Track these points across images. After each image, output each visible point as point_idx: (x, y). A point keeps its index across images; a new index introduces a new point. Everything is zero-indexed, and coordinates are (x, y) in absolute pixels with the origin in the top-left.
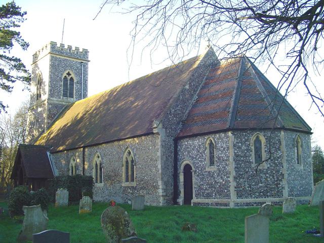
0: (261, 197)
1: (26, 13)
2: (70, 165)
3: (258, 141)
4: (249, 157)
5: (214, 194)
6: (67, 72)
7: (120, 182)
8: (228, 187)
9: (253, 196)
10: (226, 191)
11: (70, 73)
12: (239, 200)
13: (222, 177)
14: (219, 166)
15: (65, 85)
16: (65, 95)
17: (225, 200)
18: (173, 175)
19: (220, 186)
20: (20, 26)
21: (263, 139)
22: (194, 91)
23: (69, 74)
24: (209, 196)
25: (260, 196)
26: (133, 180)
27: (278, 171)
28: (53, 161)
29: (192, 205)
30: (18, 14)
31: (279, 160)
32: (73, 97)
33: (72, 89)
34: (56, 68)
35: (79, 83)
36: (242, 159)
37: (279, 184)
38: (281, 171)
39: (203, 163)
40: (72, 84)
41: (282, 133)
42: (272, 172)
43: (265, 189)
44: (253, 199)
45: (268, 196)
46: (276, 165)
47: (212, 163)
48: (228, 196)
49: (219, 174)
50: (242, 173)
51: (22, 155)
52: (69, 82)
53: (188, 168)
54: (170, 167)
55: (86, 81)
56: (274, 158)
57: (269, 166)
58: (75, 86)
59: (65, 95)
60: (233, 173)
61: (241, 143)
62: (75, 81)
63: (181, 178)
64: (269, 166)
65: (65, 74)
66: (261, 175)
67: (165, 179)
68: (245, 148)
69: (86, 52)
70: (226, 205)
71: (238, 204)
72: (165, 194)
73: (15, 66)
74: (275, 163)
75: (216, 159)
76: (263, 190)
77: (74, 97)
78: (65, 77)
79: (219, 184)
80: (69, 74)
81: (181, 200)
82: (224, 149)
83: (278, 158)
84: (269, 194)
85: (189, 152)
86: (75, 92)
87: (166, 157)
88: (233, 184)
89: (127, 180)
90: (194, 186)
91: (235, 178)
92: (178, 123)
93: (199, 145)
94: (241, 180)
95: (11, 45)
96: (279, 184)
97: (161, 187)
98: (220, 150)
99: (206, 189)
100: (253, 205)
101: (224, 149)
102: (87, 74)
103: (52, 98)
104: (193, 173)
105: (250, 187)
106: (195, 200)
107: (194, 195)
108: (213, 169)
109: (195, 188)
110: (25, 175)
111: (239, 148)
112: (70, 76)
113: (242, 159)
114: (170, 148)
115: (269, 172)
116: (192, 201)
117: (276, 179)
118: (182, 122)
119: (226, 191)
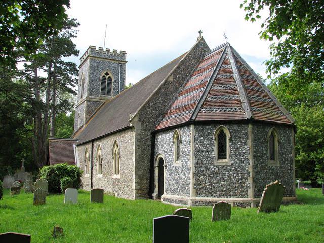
0: (223, 196)
1: (79, 24)
4: (212, 152)
6: (106, 72)
9: (214, 194)
10: (187, 188)
11: (109, 73)
15: (103, 84)
16: (103, 93)
17: (185, 198)
20: (76, 37)
23: (107, 74)
25: (221, 196)
26: (109, 93)
30: (75, 26)
31: (245, 156)
32: (110, 95)
34: (94, 69)
40: (110, 83)
41: (250, 126)
42: (236, 169)
43: (228, 187)
44: (214, 199)
46: (242, 162)
47: (178, 159)
50: (202, 169)
53: (161, 161)
54: (146, 161)
59: (103, 93)
62: (113, 80)
64: (233, 162)
65: (104, 74)
66: (224, 172)
67: (140, 173)
69: (124, 53)
71: (196, 202)
72: (139, 187)
75: (181, 154)
76: (225, 189)
77: (112, 94)
78: (104, 77)
80: (107, 74)
81: (155, 195)
83: (244, 153)
84: (231, 193)
86: (112, 90)
87: (142, 151)
88: (191, 181)
90: (164, 180)
96: (244, 183)
97: (134, 181)
102: (124, 74)
104: (165, 168)
105: (211, 185)
108: (178, 164)
109: (165, 183)
114: (147, 141)
115: (233, 169)
117: (240, 177)
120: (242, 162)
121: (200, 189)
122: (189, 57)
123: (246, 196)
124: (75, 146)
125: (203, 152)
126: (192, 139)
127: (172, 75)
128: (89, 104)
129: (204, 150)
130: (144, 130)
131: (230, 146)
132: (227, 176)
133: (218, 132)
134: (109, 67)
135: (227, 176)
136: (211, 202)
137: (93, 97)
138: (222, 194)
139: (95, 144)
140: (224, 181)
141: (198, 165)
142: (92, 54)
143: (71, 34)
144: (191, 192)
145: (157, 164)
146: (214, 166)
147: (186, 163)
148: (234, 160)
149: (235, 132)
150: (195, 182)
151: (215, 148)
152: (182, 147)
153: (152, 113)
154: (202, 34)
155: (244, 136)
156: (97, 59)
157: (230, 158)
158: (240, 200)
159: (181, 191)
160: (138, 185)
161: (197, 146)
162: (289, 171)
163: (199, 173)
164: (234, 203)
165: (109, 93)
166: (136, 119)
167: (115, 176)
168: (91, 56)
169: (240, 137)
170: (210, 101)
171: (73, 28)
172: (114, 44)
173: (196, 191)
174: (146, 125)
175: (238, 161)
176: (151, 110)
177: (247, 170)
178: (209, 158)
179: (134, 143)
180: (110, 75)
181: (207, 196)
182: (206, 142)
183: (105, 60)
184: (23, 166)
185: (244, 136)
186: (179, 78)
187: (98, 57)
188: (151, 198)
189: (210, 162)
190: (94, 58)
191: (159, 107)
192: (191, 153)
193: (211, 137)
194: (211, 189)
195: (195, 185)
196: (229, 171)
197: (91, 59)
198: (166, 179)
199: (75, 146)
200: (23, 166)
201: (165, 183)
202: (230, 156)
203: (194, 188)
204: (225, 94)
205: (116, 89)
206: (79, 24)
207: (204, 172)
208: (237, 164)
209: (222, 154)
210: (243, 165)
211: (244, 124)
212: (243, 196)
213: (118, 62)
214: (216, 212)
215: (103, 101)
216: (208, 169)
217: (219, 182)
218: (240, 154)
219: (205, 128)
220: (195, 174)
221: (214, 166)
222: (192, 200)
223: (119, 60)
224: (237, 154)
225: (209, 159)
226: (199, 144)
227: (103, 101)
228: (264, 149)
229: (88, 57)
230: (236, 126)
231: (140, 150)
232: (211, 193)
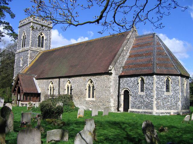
2: (49, 86)
3: (168, 81)
5: (143, 107)
7: (85, 97)
8: (152, 104)
9: (165, 109)
10: (150, 106)
11: (42, 33)
12: (158, 111)
13: (148, 99)
14: (146, 92)
15: (39, 40)
16: (39, 46)
17: (150, 111)
18: (118, 96)
19: (146, 103)
22: (128, 51)
24: (139, 108)
27: (177, 97)
28: (37, 83)
29: (129, 112)
36: (160, 89)
37: (177, 103)
38: (178, 97)
39: (137, 90)
40: (43, 40)
42: (174, 97)
43: (171, 105)
45: (172, 109)
47: (142, 90)
48: (152, 108)
49: (146, 97)
51: (20, 79)
52: (41, 39)
56: (176, 90)
57: (173, 93)
58: (44, 41)
59: (39, 46)
60: (155, 97)
61: (160, 81)
62: (45, 38)
63: (122, 97)
68: (161, 84)
70: (150, 113)
73: (6, 27)
74: (175, 92)
75: (144, 89)
78: (40, 36)
79: (146, 102)
80: (41, 34)
82: (150, 83)
84: (172, 108)
85: (128, 84)
88: (155, 102)
89: (89, 97)
91: (156, 99)
92: (120, 68)
93: (135, 81)
94: (159, 100)
95: (4, 15)
96: (177, 103)
98: (147, 84)
99: (138, 104)
100: (164, 114)
101: (150, 83)
103: (32, 47)
104: (130, 95)
105: (163, 104)
106: (130, 109)
107: (130, 107)
110: (22, 91)
111: (159, 83)
112: (42, 36)
113: (160, 89)
116: (129, 110)
118: (123, 67)
119: (150, 106)
124: (34, 79)
128: (31, 52)
129: (160, 87)
130: (116, 75)
145: (122, 92)
148: (173, 93)
151: (165, 87)
165: (42, 47)
168: (33, 22)
180: (43, 35)
196: (171, 98)
198: (131, 101)
199: (34, 79)
205: (46, 44)
218: (176, 90)
224: (175, 91)
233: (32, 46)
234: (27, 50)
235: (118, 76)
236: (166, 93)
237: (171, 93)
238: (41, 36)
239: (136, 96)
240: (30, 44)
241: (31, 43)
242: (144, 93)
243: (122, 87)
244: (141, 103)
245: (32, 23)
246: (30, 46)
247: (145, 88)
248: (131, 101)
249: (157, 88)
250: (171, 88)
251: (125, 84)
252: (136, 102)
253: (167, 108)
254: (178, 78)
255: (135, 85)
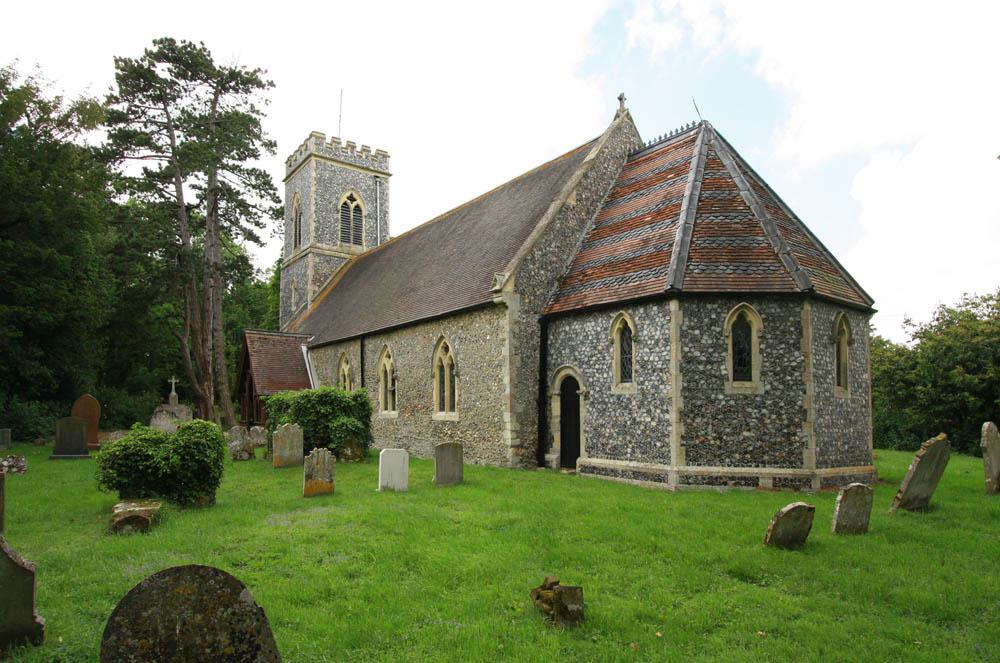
1: (271, 84)
3: (742, 327)
5: (629, 450)
6: (348, 194)
7: (428, 410)
9: (727, 460)
10: (658, 444)
11: (355, 196)
13: (649, 412)
14: (642, 383)
15: (345, 219)
16: (345, 239)
17: (657, 467)
19: (644, 432)
21: (756, 322)
22: (588, 213)
24: (615, 453)
25: (743, 462)
26: (452, 408)
27: (791, 403)
31: (797, 374)
33: (358, 228)
35: (372, 216)
36: (701, 368)
38: (799, 403)
39: (605, 376)
40: (358, 219)
41: (807, 307)
42: (775, 404)
43: (759, 444)
46: (789, 387)
47: (626, 376)
48: (664, 457)
49: (642, 402)
50: (699, 403)
53: (570, 386)
55: (385, 213)
57: (768, 387)
59: (345, 239)
63: (556, 407)
64: (768, 387)
66: (749, 410)
67: (520, 409)
68: (710, 342)
69: (385, 156)
71: (688, 477)
72: (518, 442)
75: (635, 367)
76: (751, 448)
78: (345, 203)
79: (642, 427)
80: (352, 199)
81: (553, 456)
83: (794, 368)
84: (766, 458)
86: (364, 234)
87: (522, 358)
88: (675, 431)
90: (583, 427)
93: (597, 333)
96: (795, 434)
99: (611, 436)
103: (319, 245)
104: (582, 398)
105: (721, 439)
106: (583, 459)
108: (629, 389)
109: (585, 431)
112: (355, 203)
113: (701, 368)
114: (532, 338)
115: (769, 402)
117: (786, 422)
119: (658, 444)
120: (789, 387)
121: (696, 446)
122: (603, 152)
123: (798, 463)
125: (700, 363)
126: (673, 331)
127: (575, 192)
128: (317, 260)
129: (704, 358)
130: (527, 312)
131: (761, 351)
132: (757, 418)
133: (734, 318)
134: (356, 184)
135: (757, 418)
136: (721, 478)
137: (324, 246)
138: (744, 458)
139: (370, 345)
140: (749, 430)
141: (688, 392)
142: (318, 150)
143: (252, 106)
144: (673, 455)
145: (555, 389)
146: (726, 396)
147: (656, 387)
148: (771, 383)
149: (774, 321)
150: (683, 430)
151: (729, 356)
152: (637, 353)
153: (537, 274)
154: (625, 102)
155: (792, 329)
156: (329, 163)
157: (763, 378)
158: (786, 472)
159: (638, 451)
160: (518, 437)
161: (686, 349)
162: (864, 410)
163: (692, 411)
164: (774, 479)
166: (510, 288)
167: (440, 416)
168: (316, 156)
169: (783, 332)
170: (703, 248)
171: (255, 90)
172: (360, 131)
173: (687, 451)
174: (530, 302)
175: (781, 387)
176: (538, 268)
177: (801, 407)
178: (715, 377)
179: (507, 342)
181: (709, 463)
182: (706, 340)
183: (347, 167)
184: (173, 393)
185: (792, 329)
186: (587, 199)
187: (332, 160)
188: (542, 462)
189: (715, 386)
190: (323, 161)
191: (551, 263)
192: (673, 367)
193: (718, 329)
194: (720, 448)
195: (682, 437)
196: (758, 407)
197: (317, 163)
198: (588, 423)
200: (173, 393)
201: (585, 431)
202: (763, 374)
203: (682, 445)
204: (734, 234)
206: (271, 84)
207: (703, 410)
208: (778, 393)
209: (742, 370)
210: (792, 394)
211: (793, 302)
212: (792, 465)
213: (374, 174)
214: (844, 510)
215: (348, 256)
216: (712, 402)
217: (736, 431)
219: (704, 308)
220: (683, 415)
221: (726, 396)
222: (678, 472)
223: (375, 166)
225: (714, 380)
226: (690, 345)
227: (348, 256)
228: (828, 360)
229: (310, 156)
230: (775, 305)
231: (518, 358)
232: (719, 456)
233: (319, 239)
234: (303, 254)
235: (537, 317)
236: (733, 387)
237: (757, 385)
238: (352, 206)
239: (606, 403)
240: (313, 234)
241: (317, 229)
242: (635, 384)
243: (553, 362)
244: (624, 430)
245: (313, 158)
246: (312, 240)
247: (637, 361)
248: (588, 423)
249: (689, 362)
250: (757, 361)
251: (564, 349)
252: (603, 425)
253: (737, 456)
254: (798, 309)
255: (600, 352)
